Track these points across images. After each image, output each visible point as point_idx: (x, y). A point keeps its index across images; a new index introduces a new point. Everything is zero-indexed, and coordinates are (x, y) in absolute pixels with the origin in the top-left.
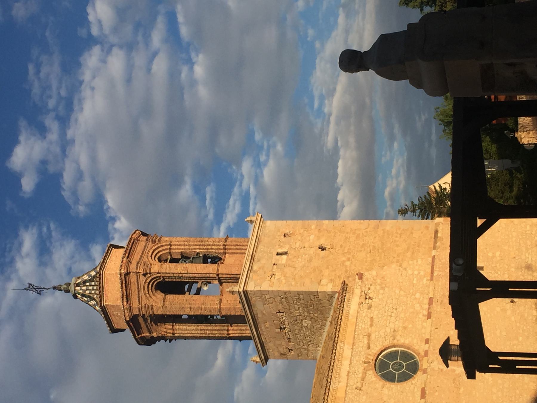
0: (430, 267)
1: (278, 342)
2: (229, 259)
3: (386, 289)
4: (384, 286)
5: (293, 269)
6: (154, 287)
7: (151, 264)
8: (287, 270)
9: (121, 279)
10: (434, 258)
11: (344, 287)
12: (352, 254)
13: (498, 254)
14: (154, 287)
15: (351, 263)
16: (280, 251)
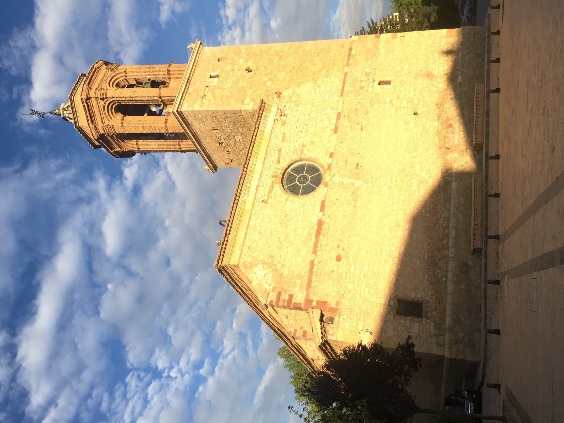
0: (341, 83)
1: (220, 154)
2: (173, 83)
3: (300, 106)
4: (298, 103)
5: (221, 91)
6: (113, 110)
7: (107, 90)
8: (217, 91)
9: (83, 103)
10: (346, 74)
11: (263, 105)
12: (274, 74)
13: (406, 67)
14: (113, 110)
15: (272, 83)
16: (213, 74)
